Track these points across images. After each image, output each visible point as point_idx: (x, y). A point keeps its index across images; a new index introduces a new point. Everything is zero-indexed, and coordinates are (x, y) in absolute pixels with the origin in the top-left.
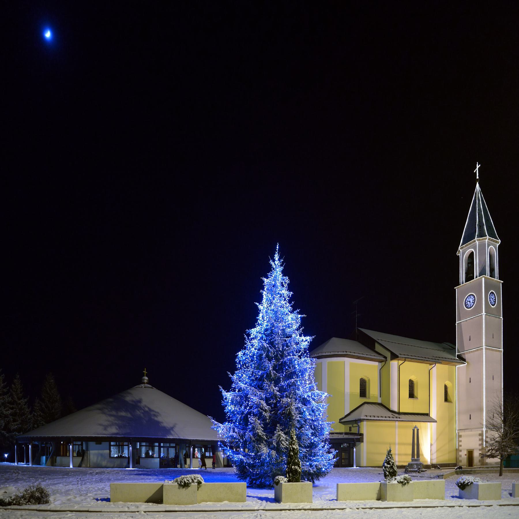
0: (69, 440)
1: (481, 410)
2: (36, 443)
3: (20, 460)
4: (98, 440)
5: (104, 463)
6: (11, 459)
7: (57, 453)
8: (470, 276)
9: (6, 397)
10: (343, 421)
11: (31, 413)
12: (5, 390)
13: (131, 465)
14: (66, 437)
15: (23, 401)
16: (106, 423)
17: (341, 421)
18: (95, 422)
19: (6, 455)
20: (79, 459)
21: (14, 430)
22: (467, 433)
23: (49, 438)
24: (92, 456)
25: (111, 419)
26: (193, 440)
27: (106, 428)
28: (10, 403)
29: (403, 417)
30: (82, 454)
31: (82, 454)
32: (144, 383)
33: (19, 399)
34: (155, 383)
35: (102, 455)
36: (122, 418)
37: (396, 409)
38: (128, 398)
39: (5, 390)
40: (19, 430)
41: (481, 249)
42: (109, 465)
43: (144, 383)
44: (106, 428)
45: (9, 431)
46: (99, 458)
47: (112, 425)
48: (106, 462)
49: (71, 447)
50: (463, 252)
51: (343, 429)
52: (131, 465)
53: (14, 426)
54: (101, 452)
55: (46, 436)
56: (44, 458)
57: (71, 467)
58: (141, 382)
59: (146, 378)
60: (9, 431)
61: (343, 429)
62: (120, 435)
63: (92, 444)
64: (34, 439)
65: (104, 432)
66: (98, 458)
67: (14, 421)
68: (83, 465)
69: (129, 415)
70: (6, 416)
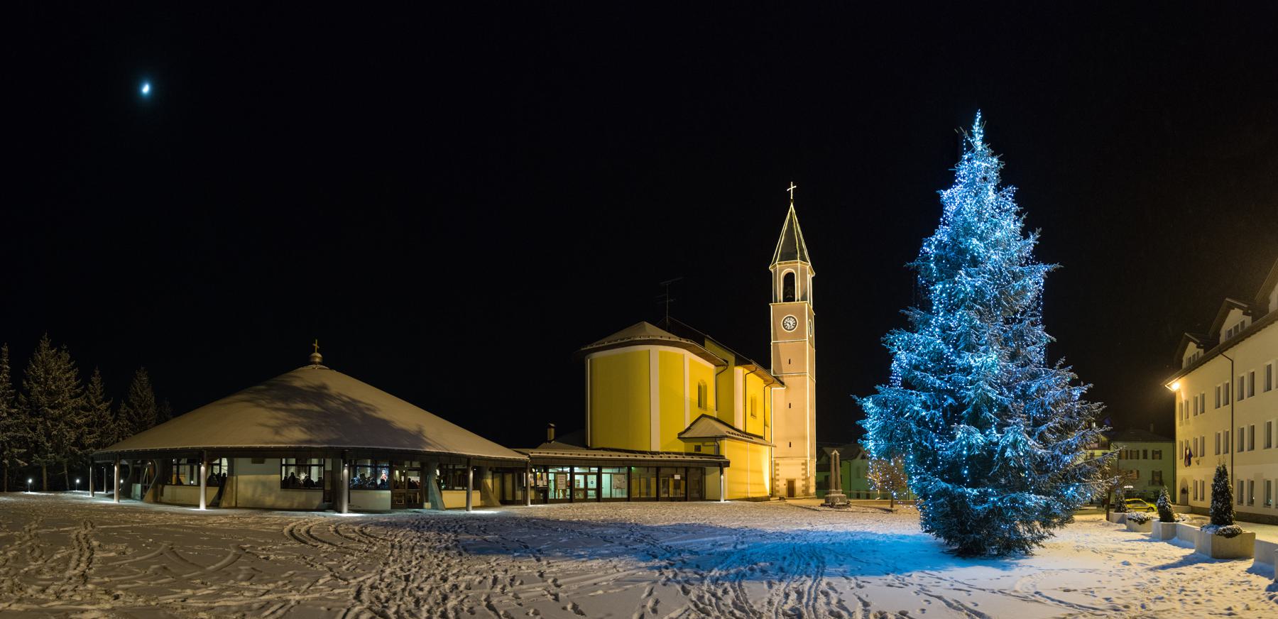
0: (196, 457)
1: (804, 438)
2: (124, 462)
3: (98, 487)
4: (258, 455)
5: (269, 500)
6: (84, 487)
7: (165, 479)
8: (789, 296)
9: (79, 400)
10: (686, 435)
11: (114, 422)
12: (78, 391)
13: (345, 508)
14: (193, 449)
15: (103, 406)
16: (273, 422)
17: (680, 436)
18: (246, 422)
19: (30, 481)
20: (214, 491)
21: (90, 445)
22: (787, 461)
23: (145, 452)
24: (241, 486)
25: (281, 414)
26: (475, 457)
27: (277, 430)
28: (84, 408)
29: (755, 440)
30: (218, 482)
31: (408, 497)
32: (315, 363)
33: (99, 403)
34: (329, 363)
35: (264, 484)
36: (305, 414)
37: (742, 428)
38: (297, 383)
39: (78, 391)
40: (98, 445)
41: (979, 116)
42: (280, 503)
43: (315, 363)
44: (277, 430)
45: (83, 447)
46: (259, 490)
47: (289, 425)
48: (273, 498)
49: (203, 468)
50: (780, 269)
51: (681, 447)
52: (345, 508)
53: (89, 440)
54: (262, 477)
55: (149, 448)
56: (139, 487)
57: (202, 508)
58: (307, 361)
59: (318, 356)
60: (83, 447)
61: (681, 447)
62: (316, 443)
63: (242, 463)
64: (122, 455)
65: (278, 438)
66: (255, 491)
67: (90, 433)
68: (224, 504)
69: (316, 408)
70: (79, 427)
